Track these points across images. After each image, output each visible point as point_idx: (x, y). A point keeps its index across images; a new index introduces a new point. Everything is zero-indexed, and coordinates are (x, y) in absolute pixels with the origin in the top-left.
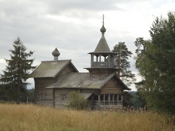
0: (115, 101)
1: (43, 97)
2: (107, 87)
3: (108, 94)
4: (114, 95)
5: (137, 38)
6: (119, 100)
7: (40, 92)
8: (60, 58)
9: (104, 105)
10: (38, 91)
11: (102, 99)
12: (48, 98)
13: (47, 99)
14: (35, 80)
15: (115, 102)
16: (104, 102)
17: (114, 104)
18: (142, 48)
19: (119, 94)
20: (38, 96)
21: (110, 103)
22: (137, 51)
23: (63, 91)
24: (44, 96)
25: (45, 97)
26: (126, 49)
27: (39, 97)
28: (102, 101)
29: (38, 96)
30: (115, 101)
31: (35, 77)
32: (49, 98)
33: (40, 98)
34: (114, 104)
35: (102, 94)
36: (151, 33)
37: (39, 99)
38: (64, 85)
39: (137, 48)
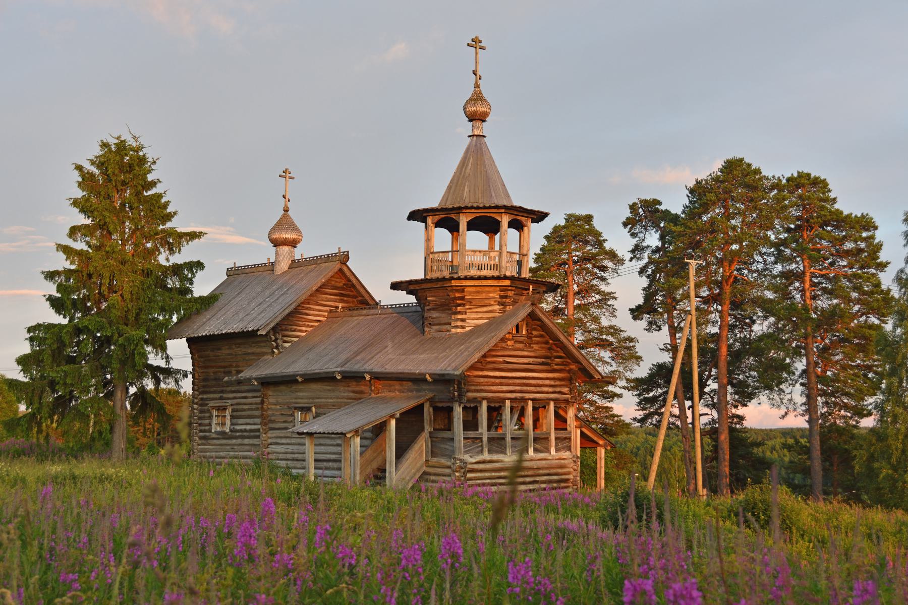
0: (493, 433)
1: (223, 424)
2: (492, 366)
3: (503, 400)
4: (530, 403)
5: (635, 204)
6: (466, 428)
7: (212, 404)
8: (303, 251)
9: (482, 451)
10: (205, 396)
11: (471, 424)
12: (243, 427)
13: (241, 431)
14: (189, 347)
15: (490, 440)
16: (485, 439)
17: (486, 450)
18: (653, 239)
19: (556, 400)
20: (207, 422)
21: (515, 442)
22: (637, 250)
23: (300, 391)
24: (228, 417)
25: (235, 421)
26: (600, 243)
27: (210, 425)
28: (471, 434)
29: (207, 422)
30: (493, 433)
31: (189, 336)
32: (248, 427)
33: (214, 425)
34: (486, 450)
35: (475, 400)
36: (618, 416)
37: (210, 431)
38: (299, 366)
39: (634, 241)
